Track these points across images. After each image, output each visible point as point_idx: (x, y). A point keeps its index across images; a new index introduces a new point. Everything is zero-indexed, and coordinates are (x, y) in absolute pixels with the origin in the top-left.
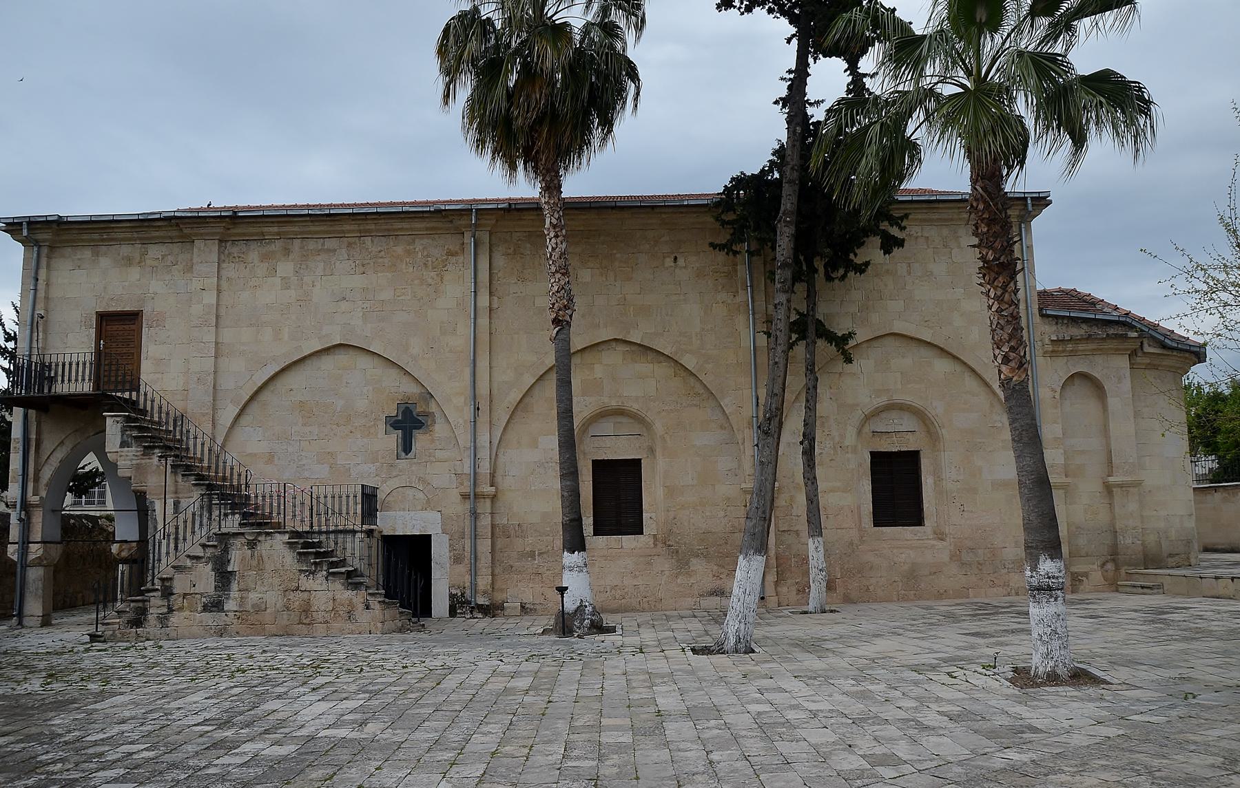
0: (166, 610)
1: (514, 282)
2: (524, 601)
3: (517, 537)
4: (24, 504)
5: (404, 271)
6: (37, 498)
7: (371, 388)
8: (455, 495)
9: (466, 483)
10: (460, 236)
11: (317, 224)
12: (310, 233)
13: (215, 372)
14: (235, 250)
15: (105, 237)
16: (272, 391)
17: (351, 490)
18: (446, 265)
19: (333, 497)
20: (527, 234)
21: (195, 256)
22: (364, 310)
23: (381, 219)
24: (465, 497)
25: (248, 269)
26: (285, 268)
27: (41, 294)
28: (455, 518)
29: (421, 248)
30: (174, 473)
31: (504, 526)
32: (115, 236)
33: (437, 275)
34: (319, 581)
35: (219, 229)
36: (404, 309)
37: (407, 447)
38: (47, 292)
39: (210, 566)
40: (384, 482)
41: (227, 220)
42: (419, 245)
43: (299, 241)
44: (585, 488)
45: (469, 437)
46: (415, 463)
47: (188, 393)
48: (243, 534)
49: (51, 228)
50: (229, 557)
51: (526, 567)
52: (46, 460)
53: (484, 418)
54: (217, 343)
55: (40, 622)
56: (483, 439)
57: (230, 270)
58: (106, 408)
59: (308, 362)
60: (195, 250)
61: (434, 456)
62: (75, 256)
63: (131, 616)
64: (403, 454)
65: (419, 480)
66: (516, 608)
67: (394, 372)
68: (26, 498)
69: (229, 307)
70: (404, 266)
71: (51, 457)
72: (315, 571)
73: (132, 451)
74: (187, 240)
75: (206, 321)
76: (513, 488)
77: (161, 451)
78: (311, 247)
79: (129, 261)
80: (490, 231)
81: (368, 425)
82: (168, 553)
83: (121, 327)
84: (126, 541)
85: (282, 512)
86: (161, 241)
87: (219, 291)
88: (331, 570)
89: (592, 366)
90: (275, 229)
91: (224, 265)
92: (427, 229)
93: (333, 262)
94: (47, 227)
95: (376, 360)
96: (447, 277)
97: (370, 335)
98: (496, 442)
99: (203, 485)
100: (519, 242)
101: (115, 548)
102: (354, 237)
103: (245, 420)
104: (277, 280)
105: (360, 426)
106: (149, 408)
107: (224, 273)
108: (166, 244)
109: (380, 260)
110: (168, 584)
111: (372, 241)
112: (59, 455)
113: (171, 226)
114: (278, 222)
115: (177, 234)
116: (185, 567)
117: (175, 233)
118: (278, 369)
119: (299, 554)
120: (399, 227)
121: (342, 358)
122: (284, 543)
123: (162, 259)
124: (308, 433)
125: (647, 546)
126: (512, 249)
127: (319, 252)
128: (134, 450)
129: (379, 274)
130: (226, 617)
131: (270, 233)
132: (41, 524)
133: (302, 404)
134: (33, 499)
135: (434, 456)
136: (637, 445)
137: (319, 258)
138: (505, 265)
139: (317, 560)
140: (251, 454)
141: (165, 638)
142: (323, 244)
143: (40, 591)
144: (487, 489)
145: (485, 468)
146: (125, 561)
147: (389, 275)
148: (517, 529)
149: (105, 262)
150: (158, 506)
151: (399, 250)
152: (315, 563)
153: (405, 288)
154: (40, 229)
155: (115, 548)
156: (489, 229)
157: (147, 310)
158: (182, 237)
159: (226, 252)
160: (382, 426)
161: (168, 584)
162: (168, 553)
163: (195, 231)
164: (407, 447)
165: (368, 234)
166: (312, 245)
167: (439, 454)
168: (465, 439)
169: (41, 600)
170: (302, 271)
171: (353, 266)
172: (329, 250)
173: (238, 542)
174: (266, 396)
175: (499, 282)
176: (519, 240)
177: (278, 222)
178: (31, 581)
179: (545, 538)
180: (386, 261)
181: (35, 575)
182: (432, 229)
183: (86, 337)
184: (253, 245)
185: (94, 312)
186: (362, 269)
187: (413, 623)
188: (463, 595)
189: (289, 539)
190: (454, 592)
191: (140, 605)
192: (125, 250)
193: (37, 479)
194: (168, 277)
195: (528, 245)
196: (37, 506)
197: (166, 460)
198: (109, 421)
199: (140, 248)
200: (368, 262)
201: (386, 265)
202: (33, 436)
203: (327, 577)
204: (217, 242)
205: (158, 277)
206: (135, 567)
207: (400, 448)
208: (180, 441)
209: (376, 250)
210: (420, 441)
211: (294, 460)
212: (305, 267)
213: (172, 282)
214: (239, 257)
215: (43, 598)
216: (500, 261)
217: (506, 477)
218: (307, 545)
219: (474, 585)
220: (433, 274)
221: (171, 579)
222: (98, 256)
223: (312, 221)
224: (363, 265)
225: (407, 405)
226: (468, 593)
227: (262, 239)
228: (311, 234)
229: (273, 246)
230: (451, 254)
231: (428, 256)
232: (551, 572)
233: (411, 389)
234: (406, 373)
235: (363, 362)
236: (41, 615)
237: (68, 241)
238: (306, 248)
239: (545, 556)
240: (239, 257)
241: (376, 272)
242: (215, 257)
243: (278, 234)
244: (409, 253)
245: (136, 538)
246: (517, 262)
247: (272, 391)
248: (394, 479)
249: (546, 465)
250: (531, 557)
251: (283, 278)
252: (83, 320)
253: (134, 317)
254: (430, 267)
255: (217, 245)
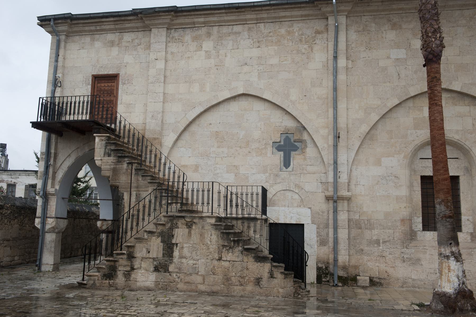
0: (128, 269)
1: (363, 50)
2: (372, 276)
3: (366, 229)
4: (45, 193)
5: (286, 45)
6: (53, 190)
7: (263, 123)
8: (321, 198)
9: (331, 189)
10: (325, 21)
11: (229, 15)
12: (225, 21)
13: (163, 112)
14: (176, 34)
15: (98, 28)
16: (198, 125)
17: (255, 190)
18: (315, 40)
19: (247, 195)
20: (373, 16)
21: (152, 38)
22: (259, 71)
23: (271, 10)
24: (328, 199)
25: (184, 46)
26: (208, 45)
27: (60, 64)
28: (321, 213)
29: (298, 29)
30: (137, 174)
31: (357, 220)
32: (104, 28)
33: (309, 47)
34: (236, 254)
35: (166, 19)
36: (286, 70)
37: (287, 163)
38: (64, 62)
39: (160, 239)
40: (271, 186)
41: (172, 13)
42: (296, 27)
43: (217, 27)
44: (415, 196)
45: (331, 157)
46: (293, 174)
47: (146, 125)
48: (183, 217)
49: (67, 22)
50: (174, 233)
51: (373, 251)
52: (60, 166)
53: (342, 143)
54: (164, 94)
55: (52, 268)
56: (343, 158)
57: (173, 47)
58: (96, 131)
59: (221, 106)
60: (152, 35)
61: (306, 170)
62: (80, 41)
63: (106, 271)
64: (285, 168)
65: (296, 186)
66: (366, 280)
67: (278, 113)
68: (46, 189)
69: (172, 70)
70: (286, 42)
71: (63, 165)
72: (233, 247)
73: (111, 160)
74: (147, 29)
75: (158, 79)
76: (363, 193)
77: (129, 159)
78: (224, 31)
79: (112, 44)
80: (346, 15)
81: (260, 148)
82: (132, 228)
83: (106, 85)
84: (105, 220)
85: (211, 203)
86: (131, 30)
87: (166, 61)
88: (246, 247)
89: (422, 108)
90: (202, 20)
91: (170, 44)
92: (302, 16)
93: (239, 40)
94: (65, 21)
95: (267, 104)
96: (316, 48)
97: (263, 88)
98: (351, 161)
99: (155, 183)
100: (367, 23)
101: (99, 224)
102: (252, 24)
103: (180, 143)
104: (203, 53)
105: (255, 149)
106: (122, 134)
107: (169, 50)
108: (134, 33)
109: (270, 38)
110: (131, 250)
111: (265, 26)
112: (68, 163)
113: (138, 19)
114: (204, 14)
115: (142, 25)
116: (143, 239)
117: (139, 24)
118: (202, 110)
119: (223, 233)
120: (284, 15)
121: (243, 103)
122: (212, 225)
123: (132, 41)
124: (221, 152)
125: (466, 241)
126: (362, 27)
127: (229, 34)
128: (111, 159)
129: (269, 47)
130: (170, 276)
131: (199, 23)
132: (55, 206)
133: (217, 134)
134: (50, 189)
135: (306, 170)
136: (456, 166)
137: (230, 38)
138: (357, 39)
139: (236, 239)
140: (184, 165)
141: (128, 289)
142: (232, 29)
143: (53, 249)
144: (343, 193)
145: (343, 178)
146: (103, 232)
147: (276, 48)
148: (366, 222)
149: (98, 44)
150: (126, 197)
151: (283, 31)
152: (234, 241)
153: (286, 56)
154: (61, 23)
155: (99, 224)
156: (346, 14)
157: (122, 73)
158: (144, 27)
159: (171, 36)
160: (270, 149)
161: (131, 250)
162: (132, 228)
163: (153, 22)
164: (287, 163)
165: (262, 21)
166: (225, 30)
167: (310, 169)
168: (328, 157)
169: (53, 254)
170: (218, 47)
171: (252, 43)
172: (236, 33)
173: (180, 223)
174: (194, 128)
175: (352, 51)
176: (367, 21)
177: (204, 14)
178: (48, 243)
179: (387, 231)
180: (274, 38)
181: (50, 238)
182: (305, 16)
183: (86, 91)
184: (188, 31)
185: (91, 75)
186: (258, 44)
187: (302, 289)
188: (326, 268)
189: (215, 222)
190: (320, 265)
191: (112, 263)
192: (110, 37)
193: (54, 178)
194: (135, 53)
195: (374, 25)
196: (53, 195)
197: (132, 166)
198: (97, 140)
199: (119, 35)
200: (261, 39)
201: (274, 41)
202: (53, 151)
203: (242, 251)
204: (165, 29)
205: (129, 53)
206: (110, 235)
207: (282, 164)
208: (141, 156)
209: (267, 32)
210: (296, 159)
211: (212, 170)
212: (220, 44)
213: (137, 56)
214: (179, 39)
215: (54, 253)
216: (353, 36)
217: (358, 186)
218: (227, 227)
219: (336, 260)
220: (306, 46)
221: (133, 247)
222: (94, 41)
223: (226, 13)
224: (258, 42)
225: (287, 135)
226: (331, 267)
227: (193, 26)
228: (225, 22)
229: (200, 31)
230: (318, 32)
231: (302, 34)
232: (392, 256)
233: (290, 124)
234: (287, 113)
235: (258, 106)
236: (53, 264)
237: (77, 32)
238: (221, 32)
239: (388, 244)
240: (179, 39)
241: (267, 46)
242: (164, 39)
243: (204, 23)
244: (289, 33)
245: (111, 218)
246: (365, 36)
247: (198, 125)
248: (278, 185)
249: (387, 178)
250: (377, 244)
251: (206, 52)
252: (84, 79)
253: (114, 78)
254: (304, 42)
255: (166, 32)
